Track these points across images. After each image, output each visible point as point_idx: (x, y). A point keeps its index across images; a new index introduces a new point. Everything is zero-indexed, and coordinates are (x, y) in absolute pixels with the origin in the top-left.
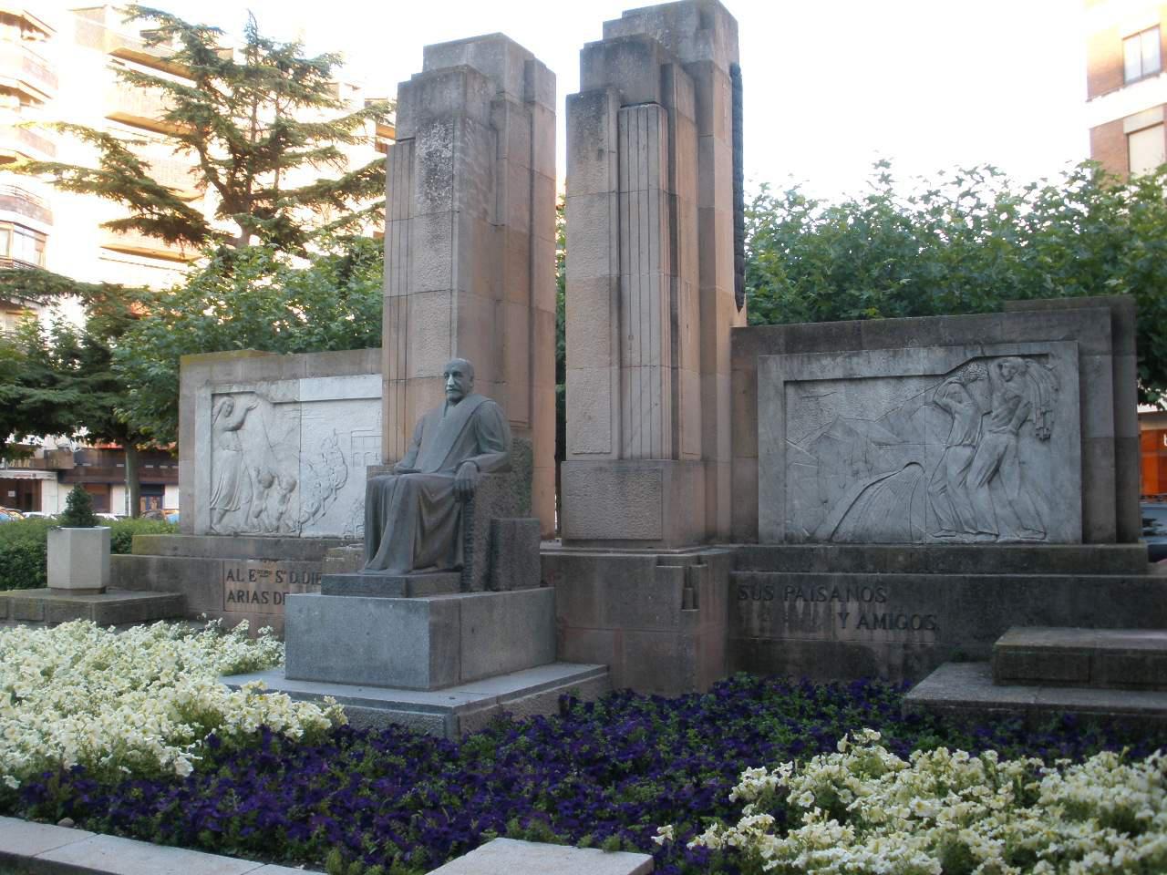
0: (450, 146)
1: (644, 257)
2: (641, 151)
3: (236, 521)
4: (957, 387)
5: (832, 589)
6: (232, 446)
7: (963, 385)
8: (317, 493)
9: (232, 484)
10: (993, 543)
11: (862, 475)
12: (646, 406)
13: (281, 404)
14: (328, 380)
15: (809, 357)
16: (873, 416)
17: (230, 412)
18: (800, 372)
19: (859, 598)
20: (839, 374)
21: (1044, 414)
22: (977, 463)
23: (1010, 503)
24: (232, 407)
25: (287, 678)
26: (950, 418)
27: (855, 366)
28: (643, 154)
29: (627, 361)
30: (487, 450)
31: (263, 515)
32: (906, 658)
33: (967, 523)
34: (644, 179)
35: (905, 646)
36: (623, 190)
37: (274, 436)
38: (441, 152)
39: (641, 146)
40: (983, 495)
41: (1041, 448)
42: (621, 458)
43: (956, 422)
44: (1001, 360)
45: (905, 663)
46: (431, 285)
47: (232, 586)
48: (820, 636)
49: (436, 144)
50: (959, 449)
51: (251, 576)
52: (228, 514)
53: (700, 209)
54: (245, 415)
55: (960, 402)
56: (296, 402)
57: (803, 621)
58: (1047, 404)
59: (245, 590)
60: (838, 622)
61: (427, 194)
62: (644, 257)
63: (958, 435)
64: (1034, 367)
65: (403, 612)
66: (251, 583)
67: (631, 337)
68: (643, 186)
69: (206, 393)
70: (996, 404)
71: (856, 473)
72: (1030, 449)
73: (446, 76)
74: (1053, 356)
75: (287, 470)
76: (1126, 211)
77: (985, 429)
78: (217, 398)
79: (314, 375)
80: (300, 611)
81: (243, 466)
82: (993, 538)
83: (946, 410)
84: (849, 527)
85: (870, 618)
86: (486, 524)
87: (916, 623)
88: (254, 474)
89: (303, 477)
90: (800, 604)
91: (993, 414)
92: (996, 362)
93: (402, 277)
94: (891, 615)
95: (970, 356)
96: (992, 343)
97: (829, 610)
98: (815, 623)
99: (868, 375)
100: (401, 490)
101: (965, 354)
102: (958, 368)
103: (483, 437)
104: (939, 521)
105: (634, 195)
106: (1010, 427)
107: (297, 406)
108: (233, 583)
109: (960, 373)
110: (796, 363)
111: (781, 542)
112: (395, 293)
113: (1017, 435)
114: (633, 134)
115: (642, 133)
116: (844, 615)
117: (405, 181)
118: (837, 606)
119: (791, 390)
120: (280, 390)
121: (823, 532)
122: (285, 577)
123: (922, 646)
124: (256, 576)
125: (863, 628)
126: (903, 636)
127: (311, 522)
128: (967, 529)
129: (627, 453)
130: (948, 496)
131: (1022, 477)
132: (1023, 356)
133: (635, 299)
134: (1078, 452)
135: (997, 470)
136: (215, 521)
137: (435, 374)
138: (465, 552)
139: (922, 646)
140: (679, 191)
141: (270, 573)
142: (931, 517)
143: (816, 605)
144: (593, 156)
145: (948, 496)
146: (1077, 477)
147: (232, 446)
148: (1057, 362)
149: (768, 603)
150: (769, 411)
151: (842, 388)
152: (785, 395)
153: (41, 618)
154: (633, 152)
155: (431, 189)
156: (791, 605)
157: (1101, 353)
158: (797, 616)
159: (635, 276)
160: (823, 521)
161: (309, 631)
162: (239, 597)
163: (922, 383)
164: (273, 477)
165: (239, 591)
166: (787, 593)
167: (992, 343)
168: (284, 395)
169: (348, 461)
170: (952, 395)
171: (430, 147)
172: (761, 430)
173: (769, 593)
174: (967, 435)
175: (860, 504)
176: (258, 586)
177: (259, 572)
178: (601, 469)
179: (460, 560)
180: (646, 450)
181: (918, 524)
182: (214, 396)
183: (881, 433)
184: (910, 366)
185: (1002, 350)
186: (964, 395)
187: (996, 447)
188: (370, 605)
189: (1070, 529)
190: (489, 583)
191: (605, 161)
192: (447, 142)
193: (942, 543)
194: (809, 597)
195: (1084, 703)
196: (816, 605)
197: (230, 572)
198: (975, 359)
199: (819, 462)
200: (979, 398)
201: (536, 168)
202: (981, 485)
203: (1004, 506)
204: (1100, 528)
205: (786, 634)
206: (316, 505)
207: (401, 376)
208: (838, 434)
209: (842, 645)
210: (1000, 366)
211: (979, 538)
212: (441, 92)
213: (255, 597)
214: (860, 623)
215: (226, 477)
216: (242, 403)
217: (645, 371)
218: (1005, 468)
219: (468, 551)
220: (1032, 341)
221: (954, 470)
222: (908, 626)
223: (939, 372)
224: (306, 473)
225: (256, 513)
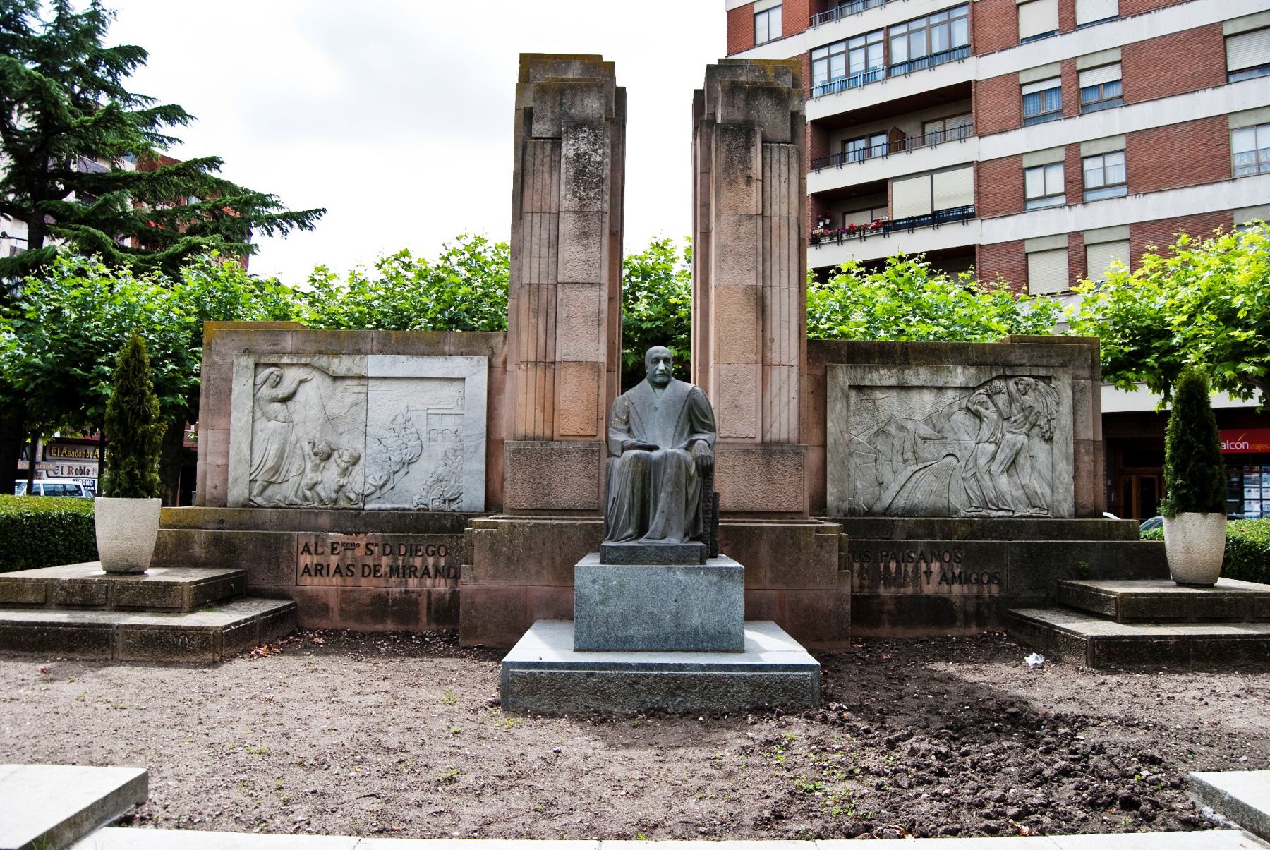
0: (600, 151)
1: (785, 274)
2: (783, 184)
3: (287, 491)
4: (985, 398)
5: (919, 552)
6: (281, 417)
7: (990, 396)
8: (386, 466)
9: (281, 456)
10: (1011, 517)
11: (911, 462)
12: (784, 399)
13: (344, 378)
14: (403, 358)
15: (869, 368)
16: (919, 417)
17: (278, 383)
18: (863, 378)
19: (941, 560)
20: (893, 382)
21: (1049, 421)
22: (1001, 456)
23: (1023, 486)
24: (281, 378)
25: (576, 650)
26: (978, 421)
28: (784, 186)
29: (768, 359)
30: (700, 430)
31: (319, 488)
32: (979, 605)
33: (991, 501)
34: (784, 207)
35: (978, 597)
36: (766, 214)
37: (333, 408)
38: (591, 156)
39: (783, 179)
40: (1003, 481)
41: (1046, 447)
42: (762, 442)
43: (984, 424)
44: (1017, 379)
45: (978, 609)
46: (580, 277)
47: (306, 560)
48: (910, 590)
49: (584, 148)
50: (986, 445)
51: (333, 549)
52: (271, 487)
54: (298, 386)
55: (987, 409)
56: (361, 377)
57: (895, 578)
58: (1052, 414)
59: (325, 565)
60: (924, 578)
61: (574, 193)
62: (785, 274)
63: (985, 433)
64: (1041, 385)
65: (715, 579)
66: (333, 557)
67: (772, 340)
68: (784, 213)
69: (249, 361)
70: (1015, 411)
71: (905, 461)
72: (1040, 448)
73: (588, 86)
75: (349, 444)
77: (1005, 431)
78: (260, 370)
79: (380, 352)
80: (594, 581)
81: (294, 438)
82: (1011, 514)
83: (977, 415)
84: (900, 502)
85: (950, 575)
87: (985, 579)
88: (307, 448)
89: (369, 451)
90: (893, 565)
91: (1013, 419)
92: (1013, 380)
93: (543, 266)
94: (965, 573)
95: (994, 374)
96: (1011, 366)
97: (916, 569)
99: (916, 384)
100: (674, 464)
101: (991, 373)
102: (986, 383)
103: (697, 418)
104: (970, 499)
105: (775, 220)
106: (1024, 430)
107: (363, 382)
108: (309, 557)
109: (987, 387)
110: (859, 373)
111: (845, 515)
112: (535, 281)
113: (1028, 435)
114: (775, 166)
115: (784, 168)
116: (928, 573)
117: (546, 176)
118: (923, 566)
119: (853, 394)
120: (341, 365)
121: (879, 507)
122: (376, 549)
123: (991, 597)
124: (339, 548)
125: (944, 584)
126: (975, 590)
127: (378, 494)
128: (990, 506)
129: (768, 438)
130: (977, 480)
131: (1032, 467)
132: (1034, 377)
133: (776, 307)
134: (1071, 450)
135: (1014, 462)
136: (255, 493)
137: (582, 360)
139: (991, 597)
141: (358, 545)
142: (964, 497)
143: (906, 566)
144: (742, 181)
145: (977, 480)
146: (1071, 469)
147: (281, 417)
148: (1057, 383)
149: (866, 565)
150: (836, 410)
151: (894, 394)
152: (848, 397)
153: (102, 601)
154: (775, 182)
155: (579, 188)
156: (885, 566)
157: (1084, 378)
158: (890, 575)
159: (776, 290)
160: (879, 499)
161: (604, 601)
162: (316, 570)
163: (958, 393)
164: (333, 450)
165: (317, 565)
166: (882, 556)
167: (1011, 366)
168: (349, 369)
169: (424, 437)
170: (981, 404)
171: (578, 149)
172: (829, 424)
173: (866, 556)
174: (993, 434)
175: (909, 486)
176: (342, 559)
177: (343, 544)
178: (748, 451)
180: (784, 436)
181: (955, 501)
182: (257, 365)
183: (925, 430)
184: (949, 379)
185: (1019, 371)
186: (990, 404)
187: (1015, 445)
188: (678, 573)
189: (1066, 508)
191: (754, 184)
192: (596, 147)
194: (901, 560)
195: (1194, 633)
196: (906, 566)
197: (306, 545)
198: (998, 377)
199: (877, 451)
200: (1001, 406)
202: (1002, 472)
203: (1018, 489)
204: (1084, 507)
205: (882, 590)
206: (385, 478)
207: (540, 358)
208: (892, 429)
209: (928, 597)
210: (1016, 384)
211: (1001, 513)
213: (338, 570)
214: (941, 580)
215: (273, 449)
216: (292, 376)
217: (785, 370)
218: (1021, 460)
221: (982, 461)
222: (979, 582)
223: (971, 385)
224: (374, 446)
225: (310, 485)
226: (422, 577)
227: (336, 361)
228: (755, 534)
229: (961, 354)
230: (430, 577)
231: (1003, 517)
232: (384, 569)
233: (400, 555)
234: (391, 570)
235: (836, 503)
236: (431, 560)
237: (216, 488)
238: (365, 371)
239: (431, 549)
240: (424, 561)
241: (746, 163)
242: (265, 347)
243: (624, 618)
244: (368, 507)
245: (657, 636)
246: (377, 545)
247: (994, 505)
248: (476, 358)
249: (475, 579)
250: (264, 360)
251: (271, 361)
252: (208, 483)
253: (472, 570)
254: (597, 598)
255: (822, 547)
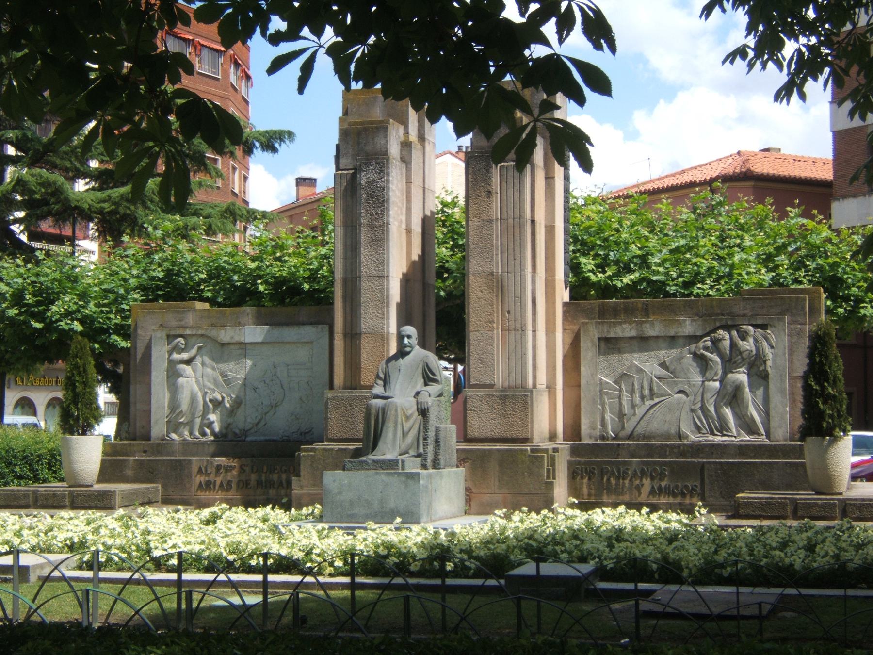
2: (515, 193)
18: (608, 332)
27: (644, 329)
39: (515, 190)
53: (546, 226)
59: (213, 481)
65: (403, 479)
74: (771, 325)
76: (817, 360)
80: (334, 481)
86: (434, 429)
95: (718, 324)
98: (623, 490)
138: (424, 446)
140: (537, 218)
158: (611, 486)
161: (340, 493)
167: (733, 315)
168: (232, 338)
179: (421, 450)
182: (168, 336)
190: (436, 465)
193: (700, 441)
201: (426, 186)
206: (259, 417)
212: (373, 139)
219: (425, 445)
220: (758, 315)
223: (698, 334)
226: (278, 488)
227: (223, 332)
228: (327, 442)
229: (692, 308)
230: (283, 488)
231: (725, 441)
232: (253, 483)
233: (263, 472)
234: (257, 484)
235: (588, 431)
236: (284, 476)
237: (143, 428)
238: (243, 338)
239: (284, 468)
240: (279, 477)
241: (487, 181)
242: (173, 323)
243: (351, 503)
244: (249, 439)
245: (370, 514)
246: (247, 466)
247: (718, 431)
248: (320, 326)
249: (301, 487)
250: (173, 333)
251: (178, 333)
252: (138, 424)
253: (300, 481)
254: (336, 491)
255: (533, 463)
